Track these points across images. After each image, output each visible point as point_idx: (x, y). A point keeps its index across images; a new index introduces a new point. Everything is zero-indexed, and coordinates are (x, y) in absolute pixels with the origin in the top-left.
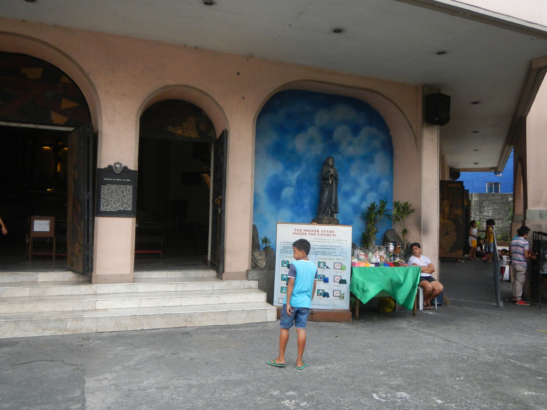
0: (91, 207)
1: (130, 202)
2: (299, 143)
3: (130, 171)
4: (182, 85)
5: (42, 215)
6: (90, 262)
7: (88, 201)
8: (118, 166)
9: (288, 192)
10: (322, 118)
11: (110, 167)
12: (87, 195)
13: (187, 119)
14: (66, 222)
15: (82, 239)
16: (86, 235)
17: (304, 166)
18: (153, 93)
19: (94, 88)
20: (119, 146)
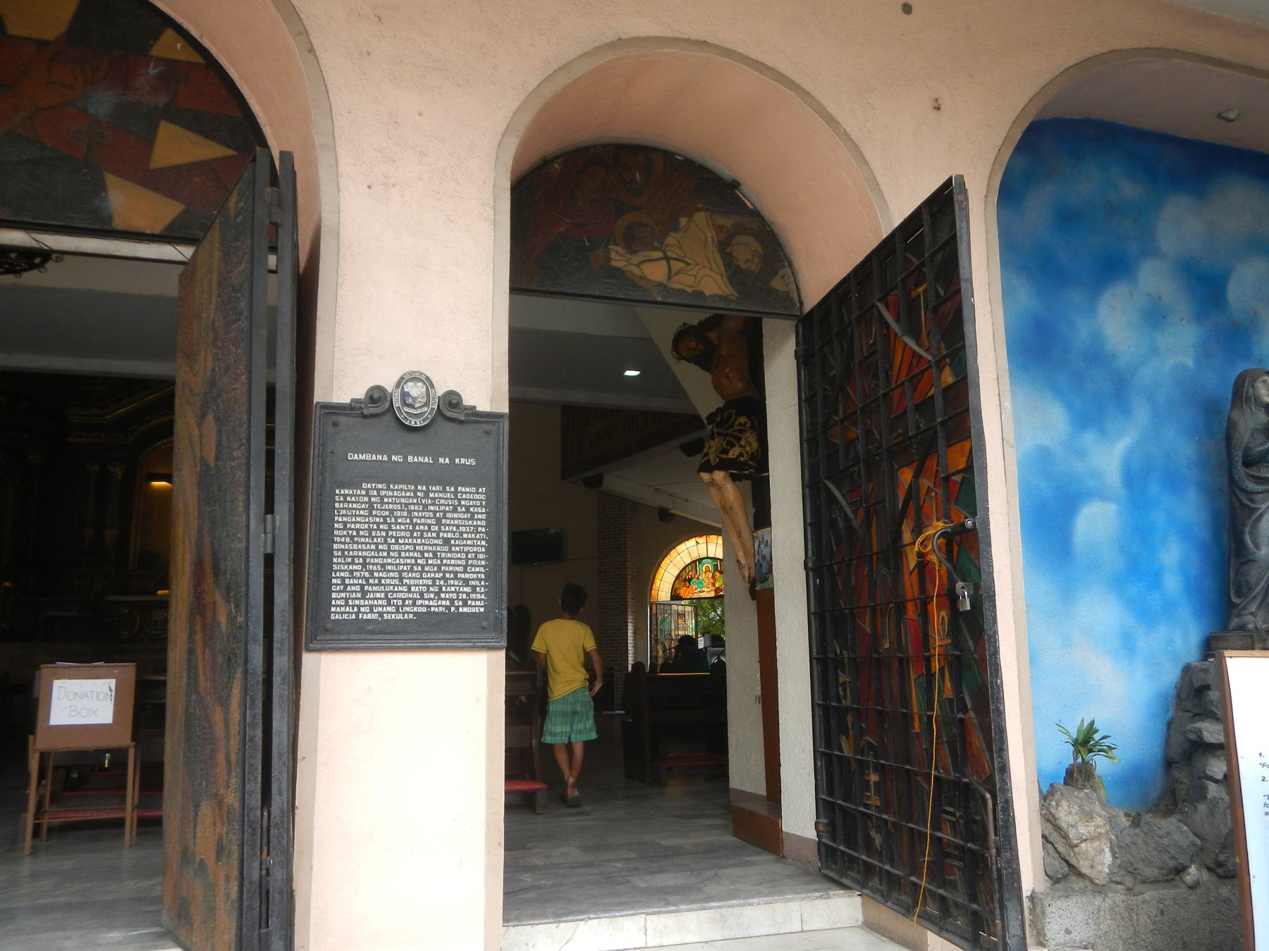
0: (282, 597)
1: (477, 572)
2: (1114, 321)
3: (476, 417)
4: (688, 40)
5: (87, 652)
6: (274, 922)
7: (269, 560)
8: (415, 390)
9: (1097, 523)
10: (1181, 225)
11: (377, 396)
12: (262, 533)
14: (164, 683)
15: (234, 782)
16: (259, 733)
17: (1142, 414)
18: (567, 66)
19: (302, 32)
20: (418, 299)
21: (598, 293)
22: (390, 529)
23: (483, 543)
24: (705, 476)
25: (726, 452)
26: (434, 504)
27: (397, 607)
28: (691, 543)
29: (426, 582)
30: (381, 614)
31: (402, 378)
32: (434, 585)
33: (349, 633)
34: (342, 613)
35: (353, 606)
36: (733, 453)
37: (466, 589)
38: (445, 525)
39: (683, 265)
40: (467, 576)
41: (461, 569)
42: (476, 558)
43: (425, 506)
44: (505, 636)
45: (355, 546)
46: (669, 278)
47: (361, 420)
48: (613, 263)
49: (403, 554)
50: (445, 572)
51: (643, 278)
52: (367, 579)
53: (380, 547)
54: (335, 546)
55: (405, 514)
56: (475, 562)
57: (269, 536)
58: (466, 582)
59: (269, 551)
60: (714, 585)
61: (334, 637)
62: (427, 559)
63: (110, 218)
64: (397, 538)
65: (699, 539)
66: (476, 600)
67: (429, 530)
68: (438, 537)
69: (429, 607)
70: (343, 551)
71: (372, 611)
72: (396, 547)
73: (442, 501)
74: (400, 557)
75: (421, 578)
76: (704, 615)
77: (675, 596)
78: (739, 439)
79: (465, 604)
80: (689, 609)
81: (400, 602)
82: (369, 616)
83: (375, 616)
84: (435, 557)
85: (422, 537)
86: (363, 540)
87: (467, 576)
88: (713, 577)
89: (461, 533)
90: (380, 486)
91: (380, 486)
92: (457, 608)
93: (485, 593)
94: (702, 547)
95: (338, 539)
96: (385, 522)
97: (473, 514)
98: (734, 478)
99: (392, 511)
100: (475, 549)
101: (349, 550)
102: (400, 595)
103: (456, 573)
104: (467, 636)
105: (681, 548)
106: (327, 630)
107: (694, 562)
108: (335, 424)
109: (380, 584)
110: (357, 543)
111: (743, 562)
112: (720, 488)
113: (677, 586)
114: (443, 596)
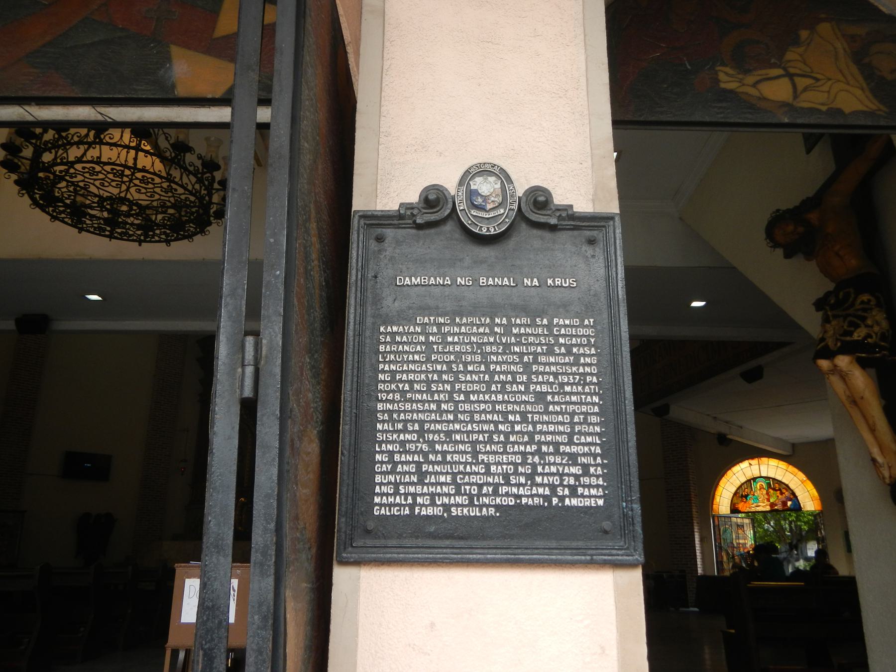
1: (590, 443)
8: (486, 186)
11: (433, 199)
13: (804, 34)
21: (707, 119)
22: (457, 380)
23: (596, 399)
24: (824, 364)
25: (851, 334)
26: (519, 344)
27: (471, 497)
28: (745, 464)
29: (512, 458)
30: (447, 507)
31: (467, 172)
32: (524, 463)
33: (400, 536)
34: (390, 505)
35: (406, 495)
36: (858, 335)
37: (574, 470)
38: (537, 373)
39: (809, 81)
40: (574, 449)
41: (563, 439)
42: (585, 422)
43: (507, 346)
44: (640, 546)
45: (408, 406)
46: (796, 96)
47: (414, 231)
48: (723, 85)
49: (477, 417)
50: (540, 443)
52: (425, 455)
53: (444, 406)
54: (380, 406)
55: (478, 358)
56: (585, 428)
57: (250, 370)
58: (573, 459)
59: (248, 392)
60: (768, 500)
61: (377, 543)
62: (513, 423)
63: (173, 86)
64: (467, 394)
65: (751, 462)
66: (590, 486)
67: (514, 381)
68: (527, 392)
69: (518, 497)
70: (390, 412)
71: (433, 504)
72: (467, 407)
73: (531, 339)
74: (472, 421)
75: (505, 452)
76: (759, 526)
77: (734, 510)
78: (864, 319)
79: (574, 493)
80: (747, 521)
81: (475, 490)
82: (430, 511)
83: (438, 511)
84: (524, 420)
85: (503, 391)
87: (574, 449)
88: (768, 494)
89: (562, 385)
90: (441, 320)
91: (441, 320)
92: (562, 499)
93: (603, 476)
96: (450, 370)
97: (577, 356)
98: (863, 364)
99: (458, 354)
100: (584, 409)
101: (399, 412)
102: (474, 479)
103: (557, 445)
104: (580, 544)
105: (736, 469)
106: (368, 532)
107: (749, 481)
109: (444, 462)
110: (411, 401)
111: (880, 459)
112: (844, 377)
113: (735, 501)
114: (539, 479)
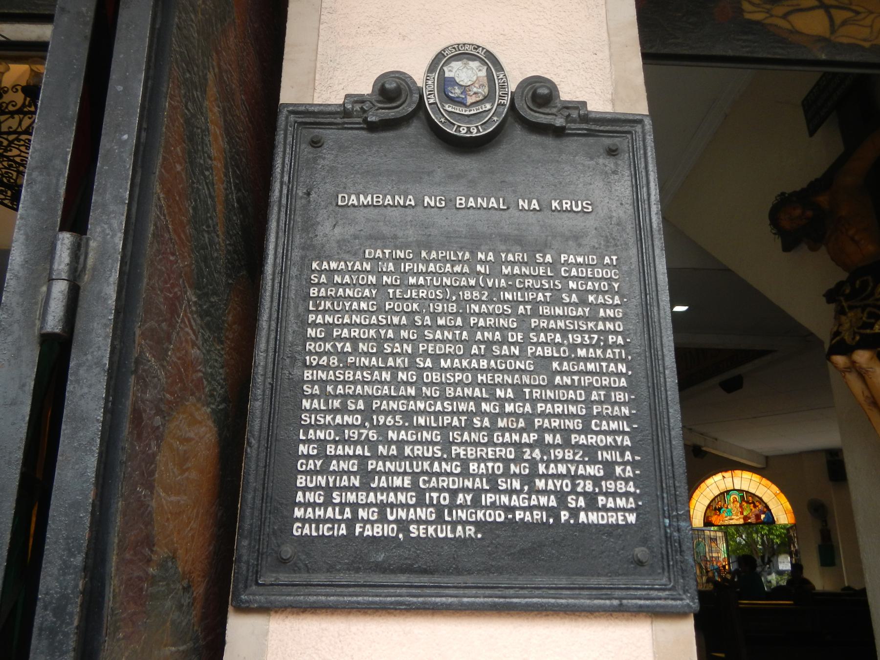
8: (467, 74)
11: (392, 89)
22: (422, 338)
26: (511, 288)
28: (718, 477)
29: (501, 452)
30: (403, 525)
31: (440, 56)
32: (518, 460)
33: (331, 569)
34: (318, 521)
35: (342, 506)
37: (592, 470)
38: (537, 330)
39: (849, 14)
40: (592, 440)
42: (607, 400)
45: (349, 375)
46: (833, 29)
47: (364, 133)
48: (747, 16)
50: (542, 430)
51: (794, 32)
56: (607, 409)
58: (590, 453)
60: (742, 513)
61: (297, 578)
62: (502, 401)
64: (436, 358)
65: (725, 474)
66: (615, 494)
67: (504, 341)
70: (323, 383)
72: (435, 377)
73: (529, 282)
74: (443, 398)
75: (491, 443)
77: (708, 523)
79: (592, 505)
80: (719, 534)
82: (377, 530)
83: (389, 530)
84: (519, 396)
85: (488, 354)
86: (365, 361)
88: (741, 507)
89: (573, 347)
94: (729, 481)
95: (313, 360)
97: (595, 307)
101: (336, 383)
102: (444, 482)
103: (567, 433)
104: (603, 581)
105: (710, 481)
106: (283, 562)
107: (722, 494)
108: (316, 143)
109: (401, 457)
110: (354, 367)
113: (708, 514)
114: (540, 484)
